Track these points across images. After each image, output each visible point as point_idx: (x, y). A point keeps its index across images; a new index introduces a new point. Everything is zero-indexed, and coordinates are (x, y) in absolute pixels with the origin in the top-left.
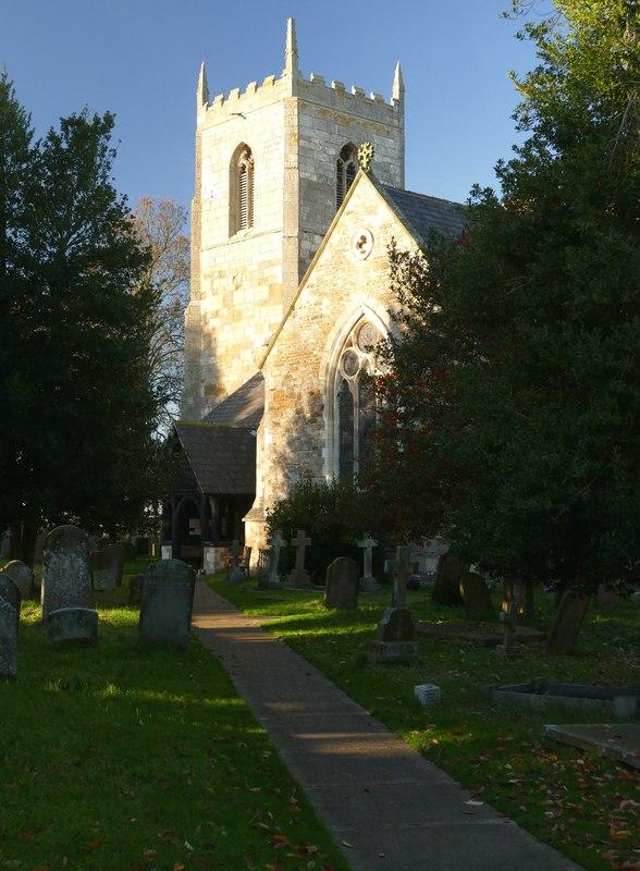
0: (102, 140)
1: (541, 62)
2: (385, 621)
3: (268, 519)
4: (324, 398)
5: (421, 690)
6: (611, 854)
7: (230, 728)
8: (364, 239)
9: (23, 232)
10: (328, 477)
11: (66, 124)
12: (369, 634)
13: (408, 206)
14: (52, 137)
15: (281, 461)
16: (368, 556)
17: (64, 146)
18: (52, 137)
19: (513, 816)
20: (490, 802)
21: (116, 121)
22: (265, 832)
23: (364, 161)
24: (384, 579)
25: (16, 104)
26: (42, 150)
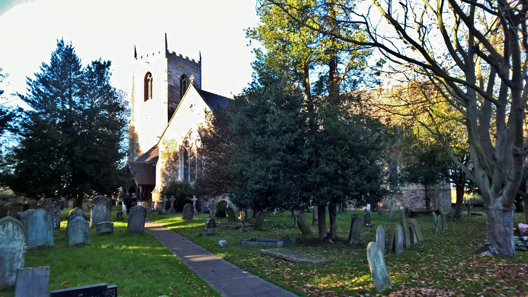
0: (107, 69)
1: (257, 59)
2: (207, 222)
3: (161, 192)
4: (179, 155)
5: (221, 242)
6: (287, 282)
7: (353, 209)
8: (192, 105)
9: (77, 98)
10: (180, 178)
11: (94, 63)
12: (202, 226)
13: (207, 97)
14: (89, 67)
15: (164, 174)
16: (194, 203)
17: (93, 70)
18: (89, 67)
19: (257, 275)
20: (250, 272)
21: (111, 63)
22: (190, 284)
23: (192, 81)
24: (199, 210)
25: (75, 55)
26: (85, 71)
